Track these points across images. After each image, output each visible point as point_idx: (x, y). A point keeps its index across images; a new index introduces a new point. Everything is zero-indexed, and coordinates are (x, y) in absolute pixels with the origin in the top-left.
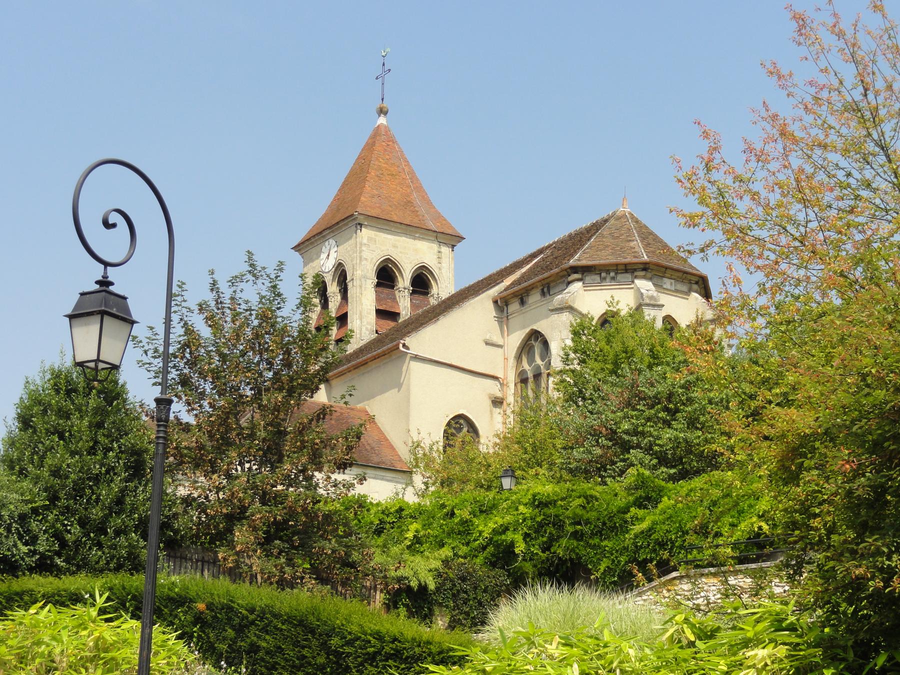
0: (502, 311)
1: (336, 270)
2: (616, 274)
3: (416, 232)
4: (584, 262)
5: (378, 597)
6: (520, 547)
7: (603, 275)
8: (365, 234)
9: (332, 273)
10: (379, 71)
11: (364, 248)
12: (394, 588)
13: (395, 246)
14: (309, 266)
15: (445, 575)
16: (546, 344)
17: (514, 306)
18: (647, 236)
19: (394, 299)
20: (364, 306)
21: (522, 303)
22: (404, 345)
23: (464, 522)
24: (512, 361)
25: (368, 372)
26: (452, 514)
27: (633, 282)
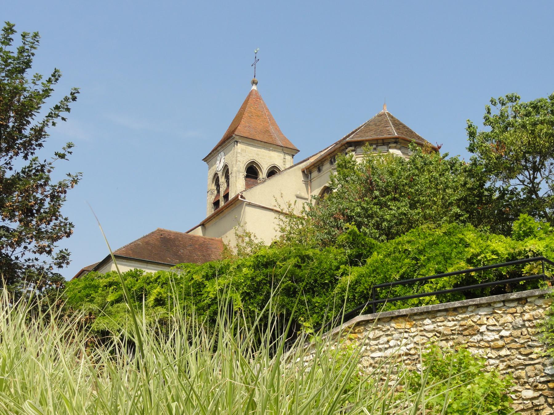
0: (308, 178)
2: (377, 146)
3: (271, 147)
4: (356, 139)
8: (240, 147)
9: (222, 171)
10: (253, 61)
11: (238, 155)
13: (258, 155)
14: (211, 169)
18: (398, 124)
21: (319, 170)
22: (242, 197)
27: (388, 151)
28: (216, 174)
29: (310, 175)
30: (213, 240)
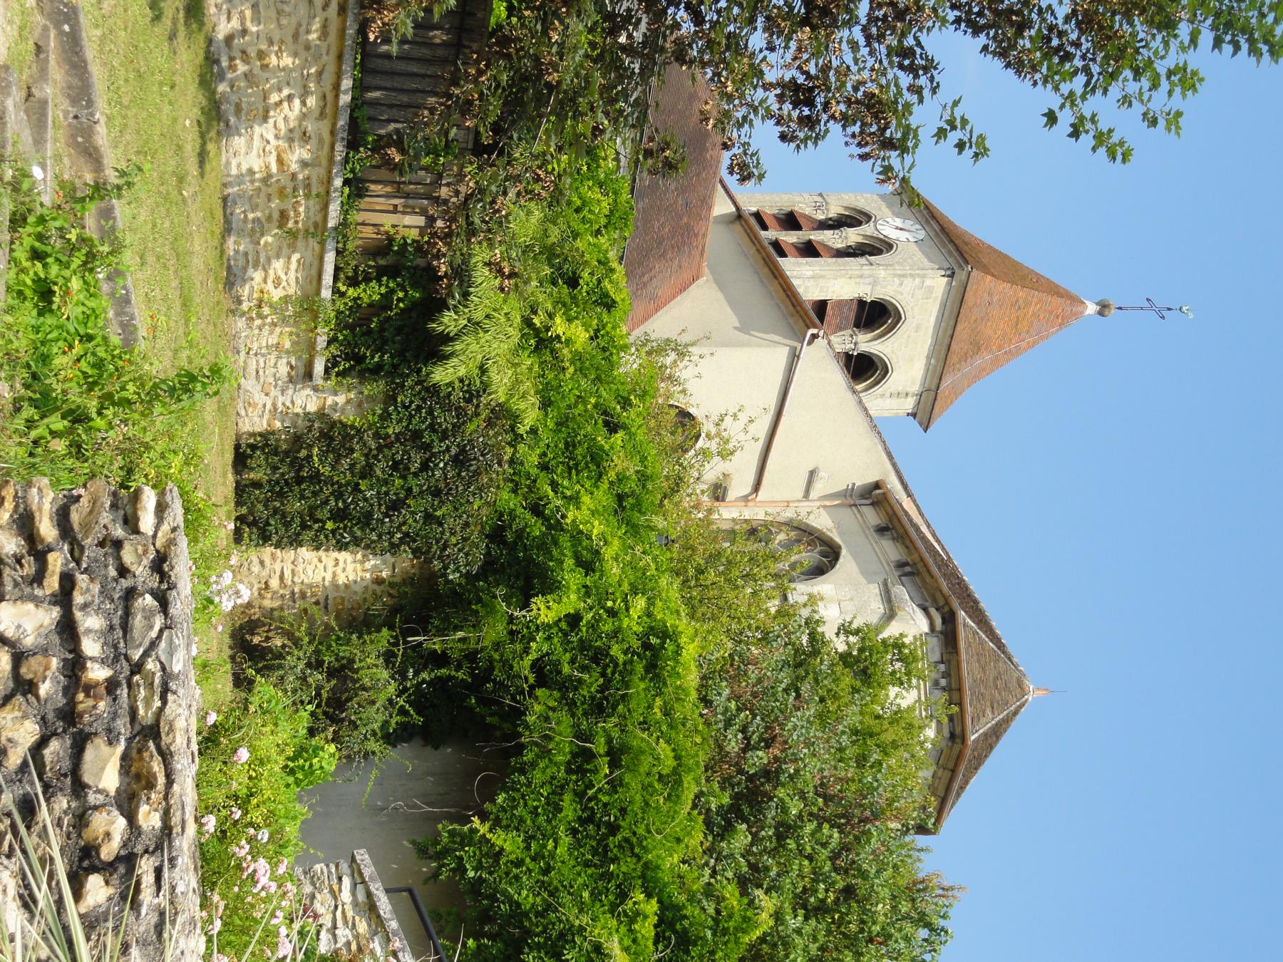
0: (863, 496)
1: (881, 240)
3: (937, 361)
5: (408, 220)
6: (546, 610)
7: (942, 667)
8: (938, 283)
9: (876, 234)
10: (1160, 302)
11: (917, 280)
12: (438, 256)
13: (918, 328)
14: (880, 202)
15: (471, 410)
16: (819, 571)
17: (872, 517)
19: (840, 328)
20: (832, 281)
21: (881, 530)
22: (814, 337)
23: (597, 458)
24: (789, 514)
25: (762, 281)
26: (612, 427)
28: (868, 217)
29: (868, 502)
30: (702, 255)
